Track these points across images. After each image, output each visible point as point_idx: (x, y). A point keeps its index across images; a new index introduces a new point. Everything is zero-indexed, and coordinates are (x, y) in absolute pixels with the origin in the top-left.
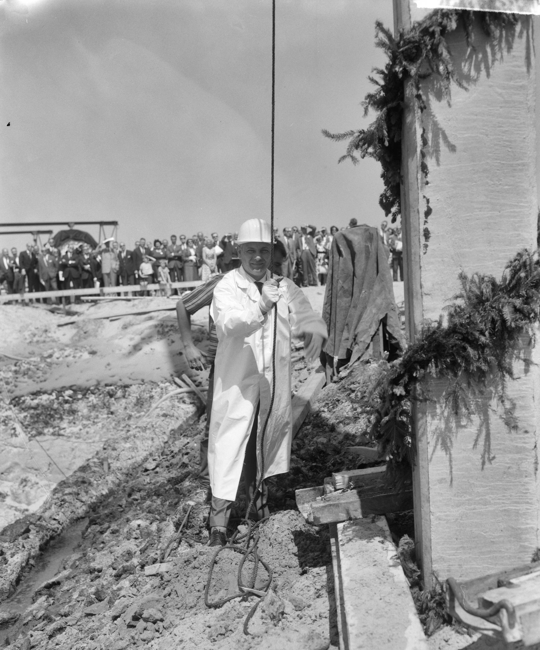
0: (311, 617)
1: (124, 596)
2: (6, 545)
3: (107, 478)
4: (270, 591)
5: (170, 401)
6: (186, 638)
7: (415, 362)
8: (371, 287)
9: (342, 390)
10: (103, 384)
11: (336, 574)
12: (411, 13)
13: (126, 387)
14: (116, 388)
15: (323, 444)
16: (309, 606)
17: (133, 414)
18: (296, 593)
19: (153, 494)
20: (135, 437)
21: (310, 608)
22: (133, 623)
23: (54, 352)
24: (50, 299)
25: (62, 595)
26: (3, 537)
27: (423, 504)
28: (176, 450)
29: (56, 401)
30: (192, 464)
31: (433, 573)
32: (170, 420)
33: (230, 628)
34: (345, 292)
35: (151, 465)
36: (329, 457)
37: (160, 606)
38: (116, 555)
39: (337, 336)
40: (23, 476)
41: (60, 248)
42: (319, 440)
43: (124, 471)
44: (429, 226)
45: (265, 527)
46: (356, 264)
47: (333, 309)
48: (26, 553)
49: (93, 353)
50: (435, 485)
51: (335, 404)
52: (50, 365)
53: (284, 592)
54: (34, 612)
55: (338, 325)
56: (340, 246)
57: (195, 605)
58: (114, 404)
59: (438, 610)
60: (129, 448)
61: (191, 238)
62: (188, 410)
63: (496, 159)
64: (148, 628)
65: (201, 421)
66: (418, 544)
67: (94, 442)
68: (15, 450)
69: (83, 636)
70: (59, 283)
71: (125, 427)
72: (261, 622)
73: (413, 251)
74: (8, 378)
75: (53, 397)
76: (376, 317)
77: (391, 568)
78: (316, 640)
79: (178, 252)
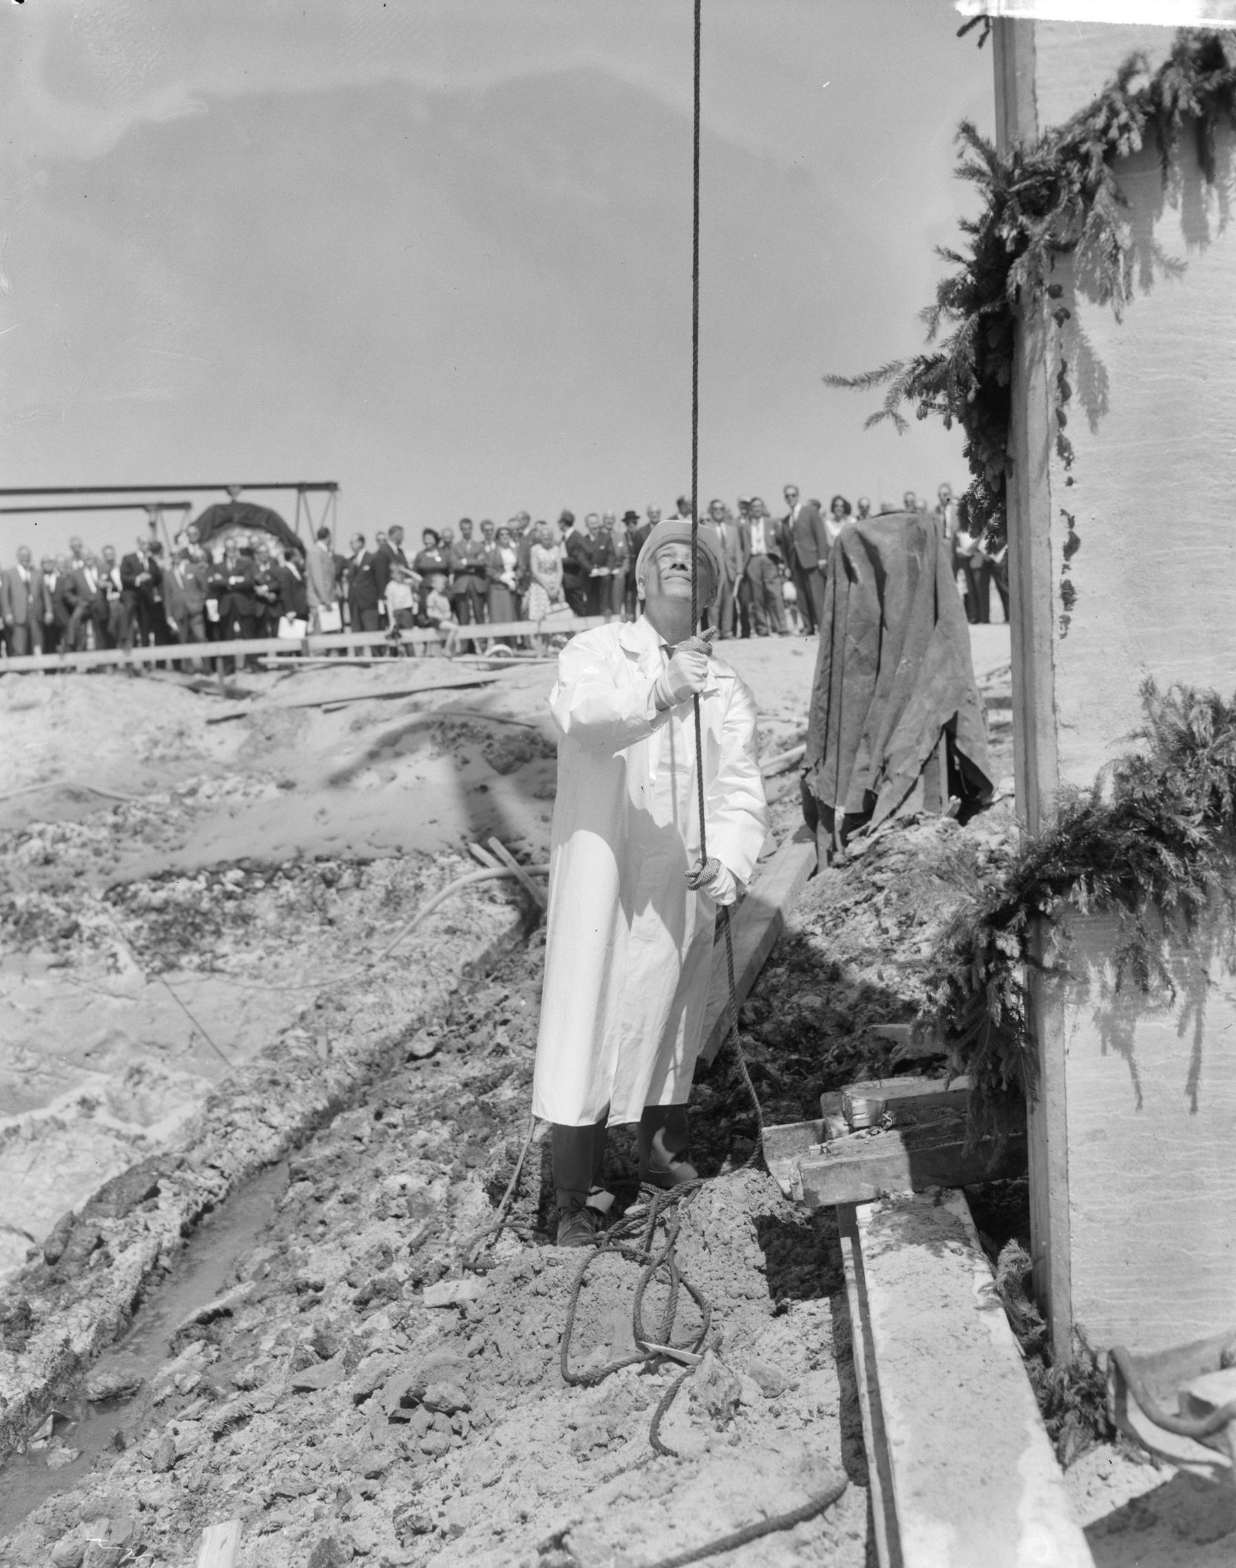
0: (798, 1413)
1: (379, 1351)
2: (108, 1223)
3: (326, 1073)
4: (710, 1354)
5: (461, 897)
6: (525, 1450)
7: (1042, 881)
8: (921, 651)
9: (855, 885)
10: (310, 855)
11: (857, 1322)
12: (1038, 106)
13: (363, 862)
14: (339, 866)
15: (813, 1010)
16: (794, 1388)
17: (377, 924)
18: (765, 1357)
19: (432, 1113)
20: (385, 980)
21: (796, 1394)
22: (403, 1413)
23: (200, 784)
24: (189, 661)
25: (237, 1341)
26: (102, 1206)
27: (1052, 1183)
28: (480, 1013)
29: (206, 893)
30: (518, 1048)
31: (1076, 1330)
32: (461, 942)
33: (618, 1432)
34: (861, 661)
35: (422, 1046)
36: (828, 1040)
37: (461, 1378)
38: (355, 1254)
39: (842, 761)
40: (135, 1061)
41: (209, 545)
42: (803, 1002)
43: (364, 1057)
44: (1074, 577)
45: (691, 1207)
46: (887, 599)
47: (835, 700)
48: (152, 1243)
49: (287, 786)
50: (1081, 1144)
51: (838, 917)
52: (191, 812)
53: (737, 1353)
54: (178, 1377)
55: (845, 736)
56: (851, 557)
57: (540, 1378)
58: (335, 901)
59: (1086, 1409)
60: (374, 1005)
61: (504, 524)
62: (501, 918)
63: (1225, 431)
64: (436, 1426)
65: (531, 946)
66: (1040, 1264)
67: (290, 988)
68: (116, 1003)
69: (289, 1436)
70: (209, 626)
71: (360, 953)
72: (688, 1420)
73: (1036, 629)
74: (99, 842)
75: (201, 884)
76: (933, 718)
77: (982, 1313)
78: (818, 1473)
79: (476, 556)
